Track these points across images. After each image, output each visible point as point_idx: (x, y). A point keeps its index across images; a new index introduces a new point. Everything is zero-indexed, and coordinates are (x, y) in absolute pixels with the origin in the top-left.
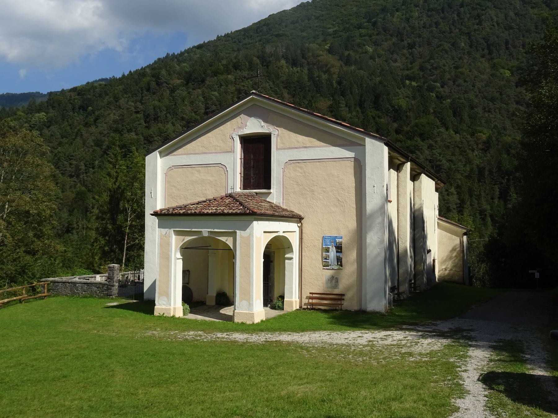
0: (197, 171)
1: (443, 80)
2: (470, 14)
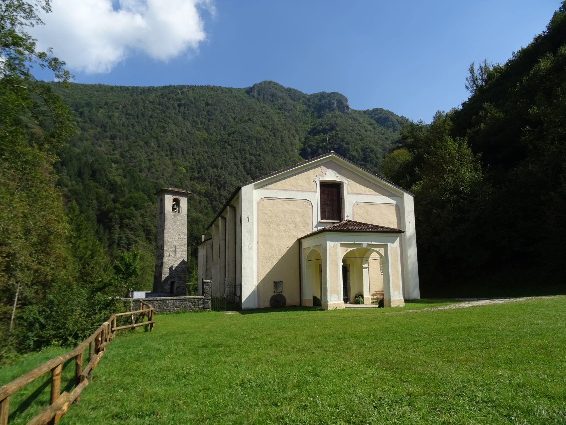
0: (287, 203)
2: (157, 124)
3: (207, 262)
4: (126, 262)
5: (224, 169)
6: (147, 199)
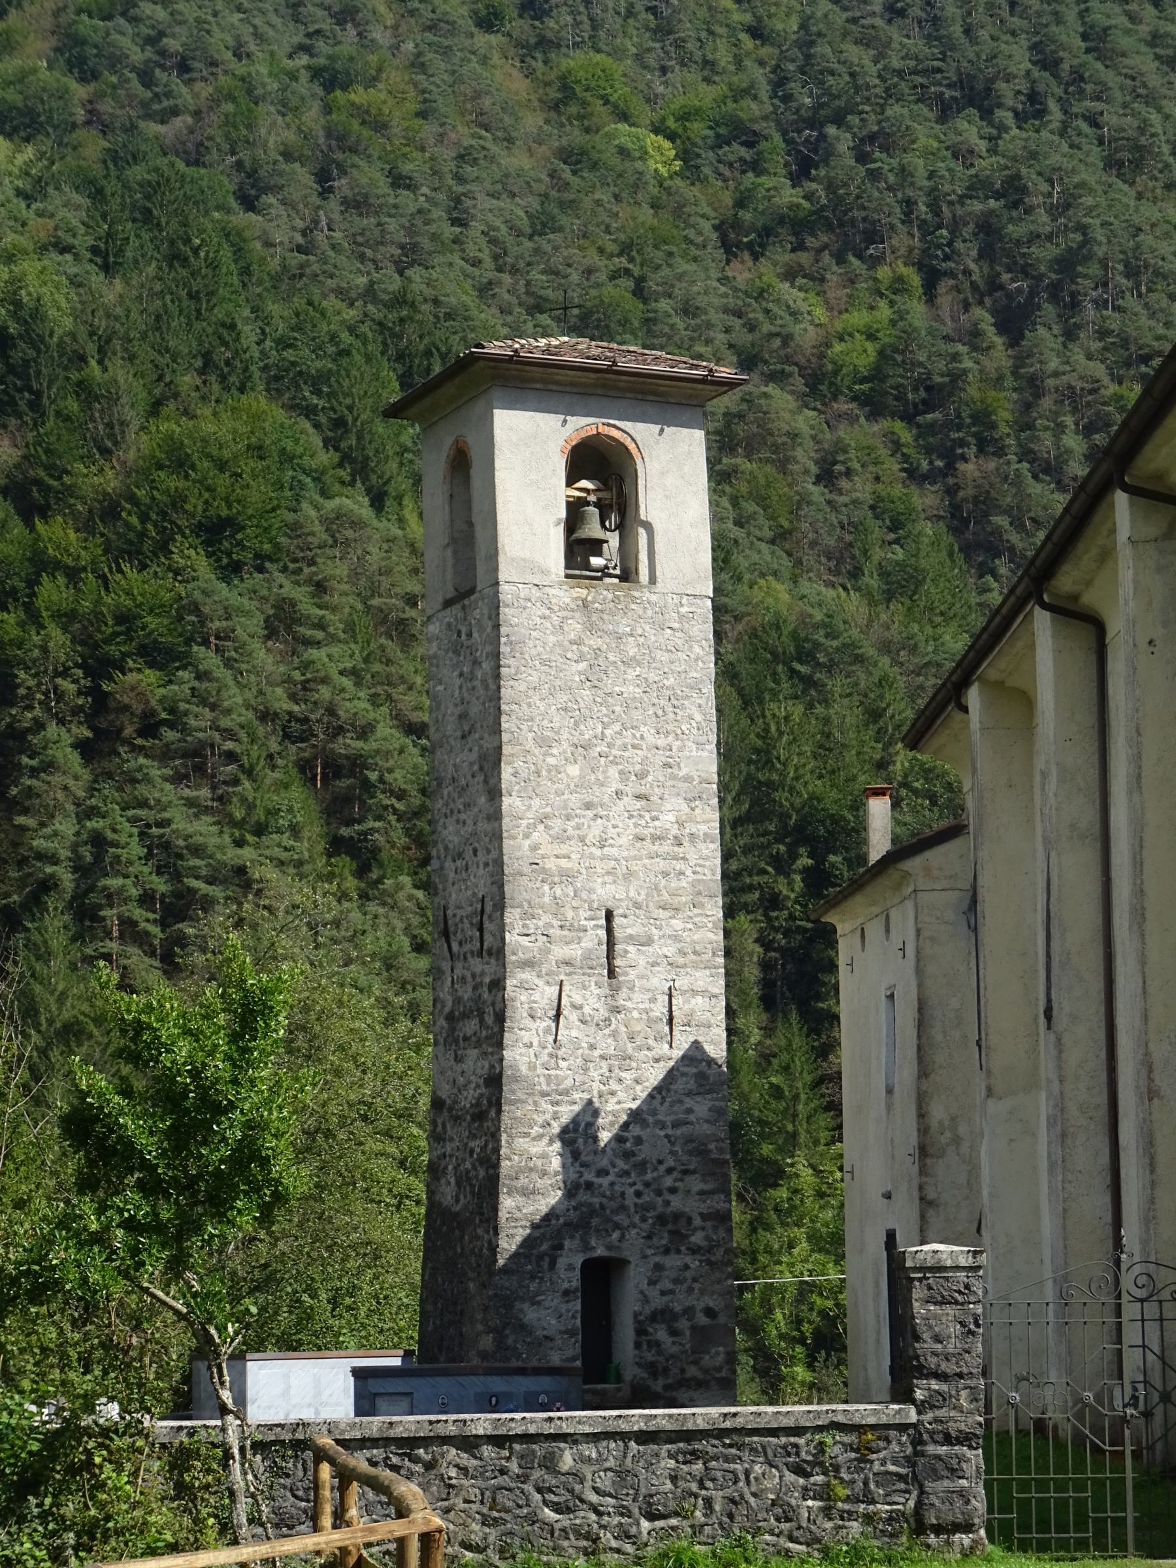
1: (244, 155)
3: (924, 1070)
4: (169, 1077)
5: (1055, 114)
6: (325, 458)
